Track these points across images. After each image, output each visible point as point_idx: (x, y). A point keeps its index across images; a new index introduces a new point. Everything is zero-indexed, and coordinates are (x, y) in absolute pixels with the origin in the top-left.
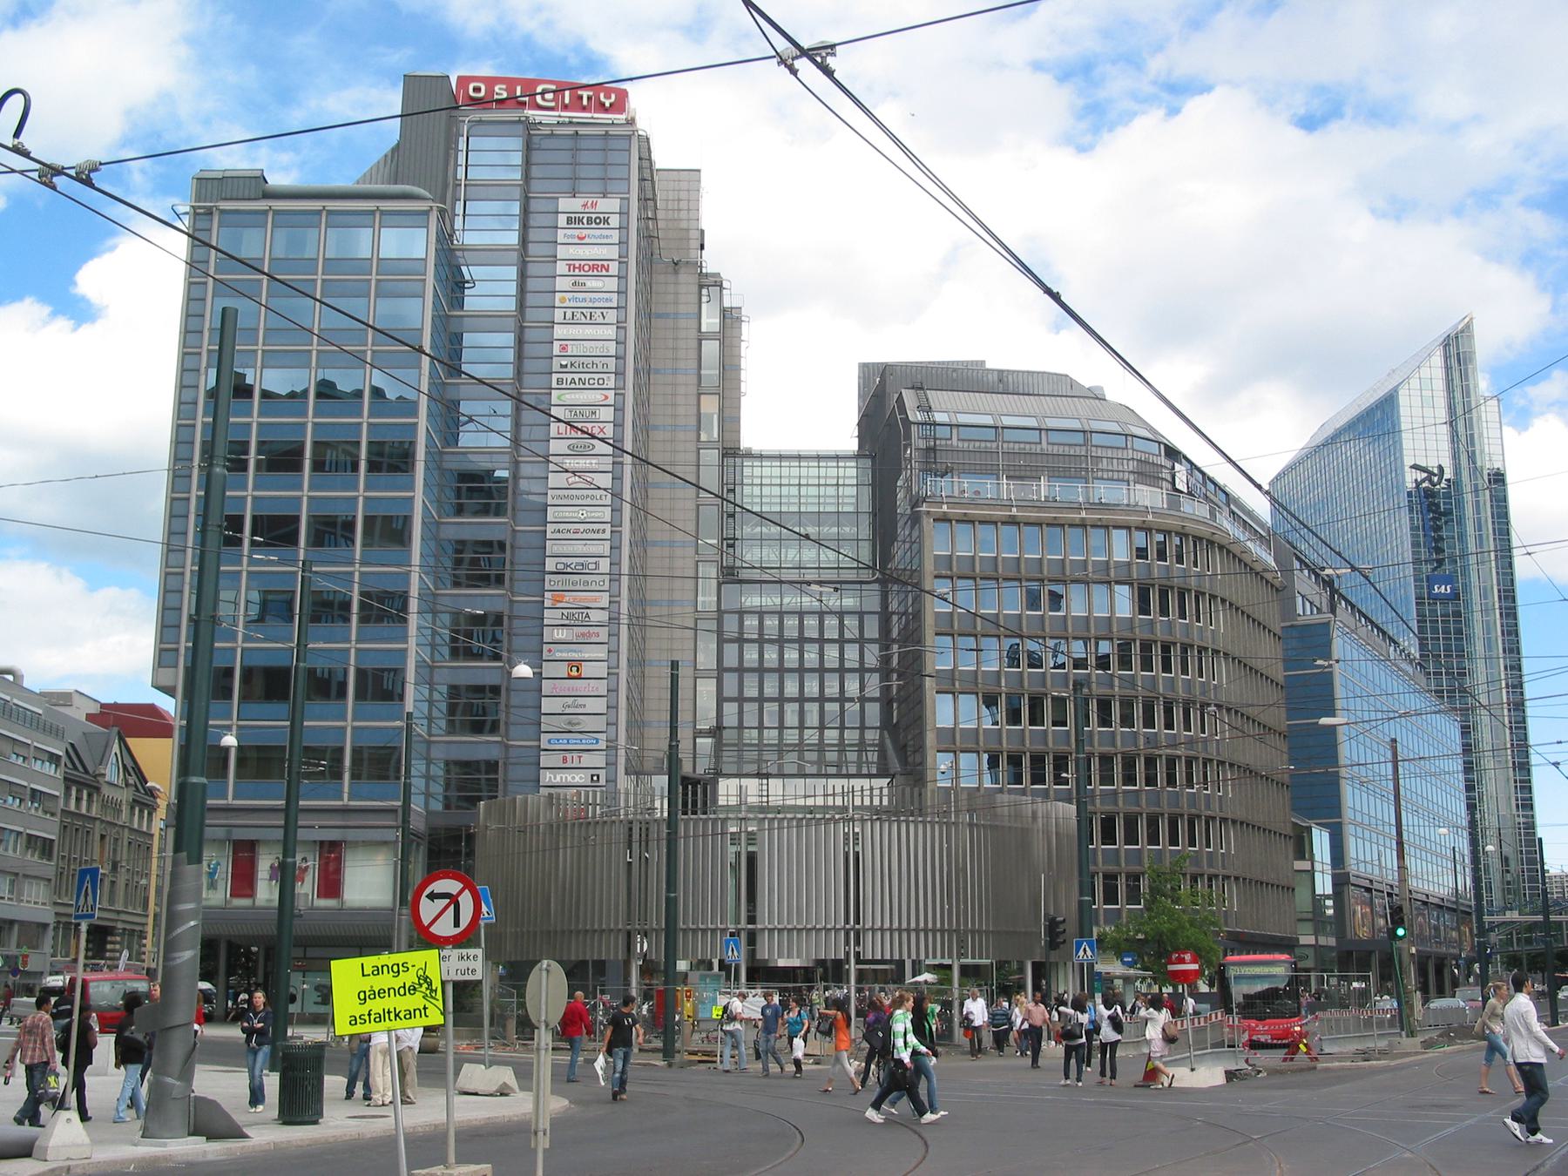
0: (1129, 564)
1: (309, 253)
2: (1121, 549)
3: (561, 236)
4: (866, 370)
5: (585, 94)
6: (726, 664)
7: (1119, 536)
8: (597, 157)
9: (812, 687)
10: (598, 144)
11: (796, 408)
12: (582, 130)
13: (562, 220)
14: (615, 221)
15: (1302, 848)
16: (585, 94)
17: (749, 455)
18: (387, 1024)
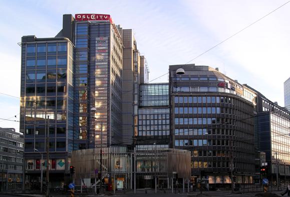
0: (219, 103)
1: (55, 51)
2: (218, 100)
3: (96, 45)
4: (170, 66)
5: (101, 16)
6: (139, 119)
7: (218, 98)
8: (103, 29)
9: (160, 122)
10: (104, 26)
11: (157, 75)
12: (100, 24)
13: (96, 42)
14: (107, 41)
15: (258, 156)
16: (101, 16)
17: (147, 85)
18: (135, 157)
